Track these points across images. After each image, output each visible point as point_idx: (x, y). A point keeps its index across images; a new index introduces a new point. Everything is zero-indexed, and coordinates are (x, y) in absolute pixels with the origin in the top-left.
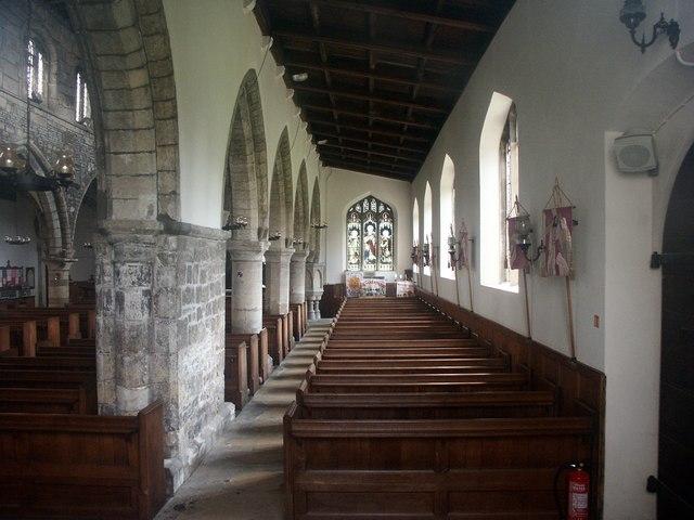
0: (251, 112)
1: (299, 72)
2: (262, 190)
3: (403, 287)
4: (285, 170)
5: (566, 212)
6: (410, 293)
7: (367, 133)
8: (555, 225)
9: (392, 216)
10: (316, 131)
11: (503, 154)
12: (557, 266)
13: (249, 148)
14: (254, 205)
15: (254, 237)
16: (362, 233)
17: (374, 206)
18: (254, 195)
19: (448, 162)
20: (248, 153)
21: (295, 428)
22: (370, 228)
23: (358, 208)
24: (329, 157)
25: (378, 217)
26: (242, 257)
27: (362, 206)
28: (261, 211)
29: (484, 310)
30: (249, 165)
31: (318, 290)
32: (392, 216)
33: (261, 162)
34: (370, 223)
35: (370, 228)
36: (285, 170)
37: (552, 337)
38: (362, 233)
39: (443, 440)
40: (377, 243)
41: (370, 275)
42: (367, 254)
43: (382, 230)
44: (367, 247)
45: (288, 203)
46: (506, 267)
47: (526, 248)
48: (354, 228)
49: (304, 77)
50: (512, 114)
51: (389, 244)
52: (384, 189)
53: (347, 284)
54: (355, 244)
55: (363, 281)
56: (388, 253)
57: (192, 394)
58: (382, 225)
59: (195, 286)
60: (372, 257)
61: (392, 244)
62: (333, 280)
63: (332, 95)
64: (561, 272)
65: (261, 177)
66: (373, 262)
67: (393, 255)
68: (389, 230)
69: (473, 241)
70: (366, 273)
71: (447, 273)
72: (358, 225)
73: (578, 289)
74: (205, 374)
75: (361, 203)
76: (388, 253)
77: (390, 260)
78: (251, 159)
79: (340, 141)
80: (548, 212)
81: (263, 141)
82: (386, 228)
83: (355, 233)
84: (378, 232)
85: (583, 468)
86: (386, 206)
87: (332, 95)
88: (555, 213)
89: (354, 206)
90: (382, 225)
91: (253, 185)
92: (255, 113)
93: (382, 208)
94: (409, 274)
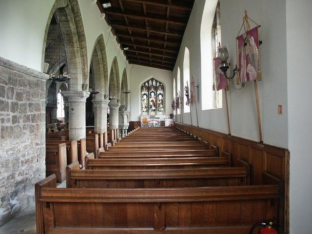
0: (75, 17)
1: (106, 2)
2: (84, 63)
3: (168, 123)
4: (103, 59)
5: (253, 32)
6: (171, 125)
7: (148, 49)
8: (246, 44)
9: (163, 88)
10: (123, 41)
11: (214, 35)
12: (248, 74)
13: (75, 38)
14: (80, 71)
15: (80, 88)
16: (149, 96)
17: (154, 83)
18: (79, 66)
19: (187, 51)
20: (74, 41)
22: (153, 94)
23: (147, 84)
24: (132, 58)
25: (156, 88)
26: (74, 100)
27: (148, 83)
28: (84, 75)
29: (204, 125)
30: (75, 49)
31: (126, 124)
32: (163, 88)
33: (83, 48)
34: (153, 92)
35: (153, 94)
36: (103, 59)
37: (245, 131)
38: (149, 96)
40: (156, 101)
41: (152, 117)
42: (151, 107)
43: (159, 95)
44: (151, 103)
45: (106, 77)
46: (214, 89)
47: (227, 73)
48: (145, 94)
49: (109, 5)
50: (218, 10)
51: (162, 101)
52: (159, 74)
53: (141, 121)
54: (145, 102)
55: (149, 120)
56: (161, 106)
57: (6, 171)
58: (158, 92)
59: (10, 101)
60: (153, 108)
61: (163, 102)
62: (134, 119)
63: (130, 30)
64: (251, 78)
65: (84, 56)
66: (154, 110)
67: (164, 107)
68: (162, 95)
69: (198, 87)
70: (151, 116)
71: (187, 109)
72: (162, 92)
73: (266, 90)
74: (22, 159)
75: (148, 82)
76: (161, 106)
77: (162, 109)
78: (76, 45)
79: (135, 47)
80: (240, 38)
81: (84, 35)
82: (160, 94)
83: (145, 96)
84: (157, 96)
85: (272, 226)
86: (160, 83)
87: (130, 30)
88: (245, 36)
89: (145, 83)
90: (158, 92)
91: (79, 60)
92: (77, 19)
93: (158, 84)
94: (172, 116)
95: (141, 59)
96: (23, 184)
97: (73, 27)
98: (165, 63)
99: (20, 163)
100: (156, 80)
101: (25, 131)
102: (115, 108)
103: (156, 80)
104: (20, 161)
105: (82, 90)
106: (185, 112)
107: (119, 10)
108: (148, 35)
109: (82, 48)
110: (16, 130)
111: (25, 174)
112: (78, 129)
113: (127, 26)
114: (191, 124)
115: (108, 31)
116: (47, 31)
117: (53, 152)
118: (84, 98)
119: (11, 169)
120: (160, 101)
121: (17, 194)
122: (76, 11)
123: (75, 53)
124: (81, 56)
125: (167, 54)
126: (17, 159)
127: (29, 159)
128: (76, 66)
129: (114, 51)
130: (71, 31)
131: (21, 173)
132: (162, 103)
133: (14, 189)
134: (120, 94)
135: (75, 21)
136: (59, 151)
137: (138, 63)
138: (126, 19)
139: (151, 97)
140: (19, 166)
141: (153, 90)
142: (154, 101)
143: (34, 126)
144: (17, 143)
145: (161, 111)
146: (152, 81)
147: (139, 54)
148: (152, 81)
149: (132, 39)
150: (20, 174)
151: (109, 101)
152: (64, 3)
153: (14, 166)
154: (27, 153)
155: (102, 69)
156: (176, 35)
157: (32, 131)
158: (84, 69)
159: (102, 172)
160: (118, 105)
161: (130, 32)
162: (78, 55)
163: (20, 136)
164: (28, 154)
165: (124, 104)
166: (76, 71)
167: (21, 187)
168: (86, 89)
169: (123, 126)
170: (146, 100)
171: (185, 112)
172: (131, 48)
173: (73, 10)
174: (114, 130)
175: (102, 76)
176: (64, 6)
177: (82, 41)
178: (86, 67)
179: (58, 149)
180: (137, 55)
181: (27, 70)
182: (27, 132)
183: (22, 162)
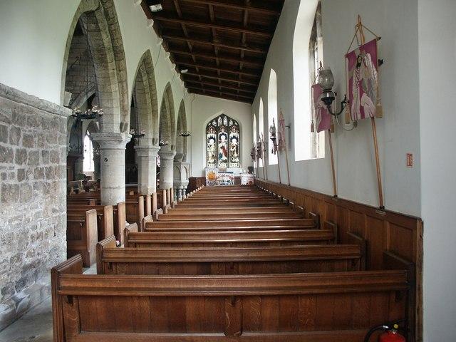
0: (110, 25)
1: (155, 3)
2: (123, 93)
3: (245, 180)
4: (150, 86)
5: (370, 47)
6: (251, 182)
7: (216, 72)
8: (359, 65)
9: (238, 129)
10: (179, 60)
11: (312, 51)
12: (362, 109)
13: (110, 56)
14: (116, 104)
15: (116, 129)
16: (217, 141)
17: (225, 121)
18: (116, 96)
19: (273, 75)
20: (109, 61)
21: (64, 284)
22: (223, 137)
23: (214, 123)
24: (193, 85)
25: (228, 129)
26: (108, 146)
27: (217, 121)
28: (123, 109)
29: (298, 182)
30: (110, 72)
31: (185, 182)
32: (238, 129)
33: (121, 69)
34: (223, 134)
35: (223, 137)
36: (150, 86)
37: (359, 191)
38: (217, 141)
39: (235, 298)
40: (228, 148)
41: (223, 171)
42: (221, 156)
43: (232, 139)
44: (221, 151)
45: (154, 112)
46: (312, 131)
47: (331, 107)
48: (212, 138)
49: (160, 7)
50: (319, 14)
51: (237, 148)
52: (232, 109)
53: (207, 177)
54: (213, 148)
55: (217, 175)
56: (236, 155)
57: (9, 251)
58: (231, 135)
59: (14, 148)
60: (224, 158)
61: (238, 149)
62: (196, 174)
63: (190, 43)
64: (367, 114)
65: (122, 82)
66: (225, 161)
67: (239, 157)
68: (237, 139)
69: (289, 127)
70: (220, 169)
71: (273, 159)
72: (236, 134)
73: (388, 132)
74: (32, 232)
75: (216, 119)
76: (236, 155)
77: (237, 160)
78: (112, 65)
79: (197, 69)
80: (350, 56)
81: (122, 52)
82: (234, 137)
83: (212, 141)
84: (229, 140)
85: (398, 330)
86: (234, 121)
87: (190, 43)
88: (358, 53)
89: (211, 122)
90: (231, 135)
91: (115, 87)
92: (113, 27)
93: (231, 123)
94: (251, 169)
95: (206, 87)
96: (34, 269)
97: (106, 39)
98: (240, 93)
99: (30, 238)
100: (227, 117)
101: (37, 192)
102: (168, 158)
103: (227, 117)
104: (29, 235)
105: (119, 132)
106: (270, 163)
107: (173, 14)
108: (216, 51)
109: (120, 71)
110: (24, 190)
111: (36, 254)
112: (114, 188)
113: (185, 37)
114: (279, 182)
115: (157, 45)
116: (69, 46)
117: (78, 222)
118: (122, 143)
119: (17, 246)
120: (233, 147)
121: (24, 284)
122: (111, 16)
123: (109, 77)
124: (119, 82)
125: (244, 78)
126: (25, 233)
127: (42, 233)
128: (111, 96)
129: (166, 74)
130: (103, 45)
131: (31, 253)
132: (237, 151)
133: (20, 277)
134: (175, 138)
135: (109, 30)
136: (86, 220)
137: (201, 93)
138: (184, 28)
139: (220, 142)
140: (28, 243)
141: (223, 132)
142: (226, 147)
143: (49, 184)
144: (25, 209)
145: (235, 162)
146: (222, 119)
147: (204, 79)
148: (222, 119)
149: (194, 58)
150: (30, 255)
151: (160, 148)
152: (93, 4)
153: (20, 242)
154: (39, 223)
155: (149, 101)
156: (258, 51)
157: (46, 192)
158: (122, 101)
159: (149, 252)
160: (172, 154)
161: (190, 47)
162: (114, 80)
163: (30, 198)
164: (41, 225)
165: (182, 152)
166: (112, 104)
167: (30, 273)
168: (125, 129)
169: (180, 184)
170: (213, 146)
171: (270, 163)
172: (191, 70)
173: (106, 14)
174: (167, 190)
175: (150, 111)
176: (94, 9)
177: (120, 60)
178: (125, 98)
179: (85, 217)
180: (201, 80)
181: (39, 103)
182: (40, 192)
183: (32, 237)
